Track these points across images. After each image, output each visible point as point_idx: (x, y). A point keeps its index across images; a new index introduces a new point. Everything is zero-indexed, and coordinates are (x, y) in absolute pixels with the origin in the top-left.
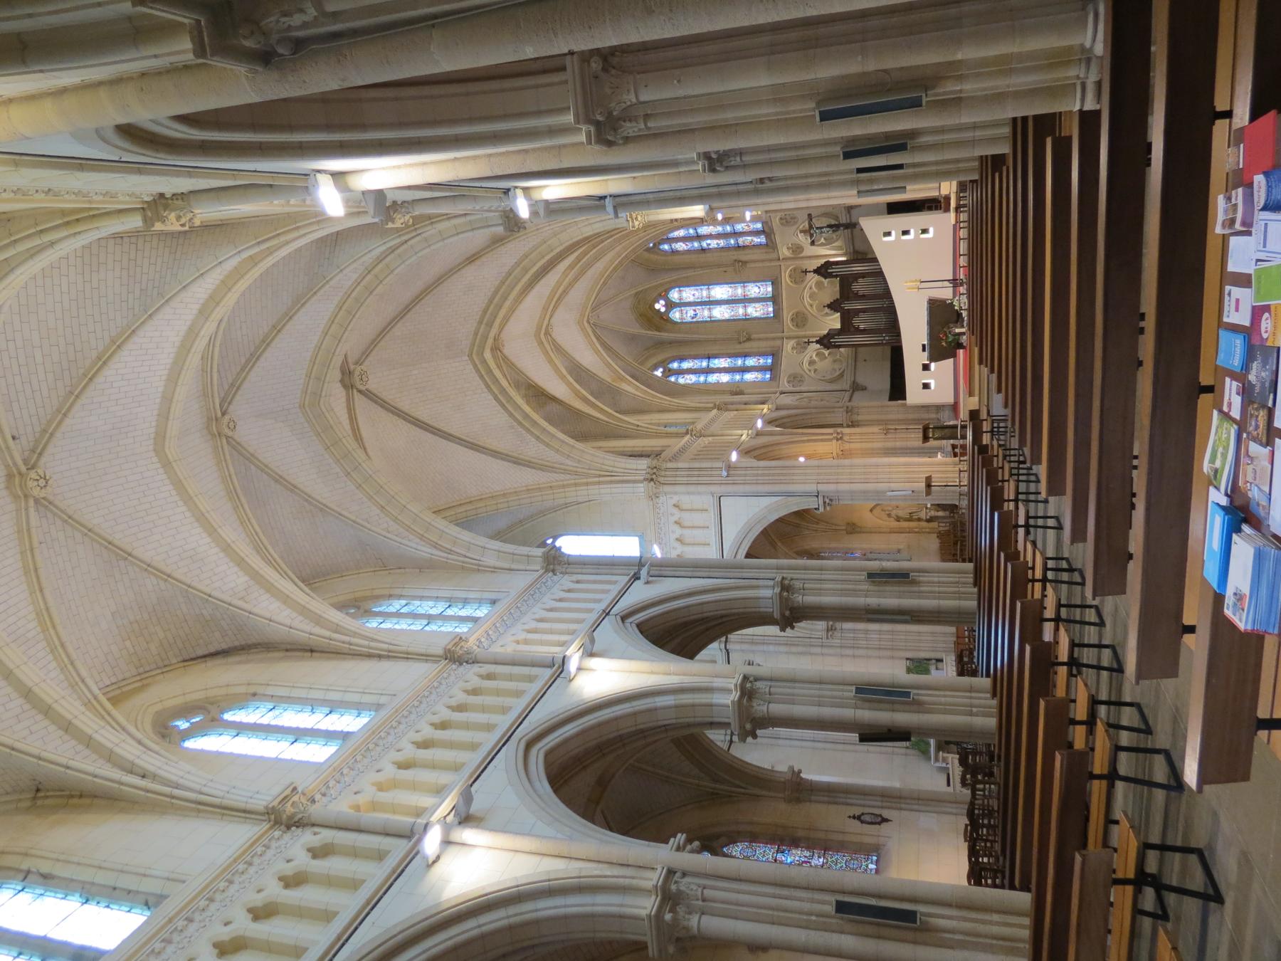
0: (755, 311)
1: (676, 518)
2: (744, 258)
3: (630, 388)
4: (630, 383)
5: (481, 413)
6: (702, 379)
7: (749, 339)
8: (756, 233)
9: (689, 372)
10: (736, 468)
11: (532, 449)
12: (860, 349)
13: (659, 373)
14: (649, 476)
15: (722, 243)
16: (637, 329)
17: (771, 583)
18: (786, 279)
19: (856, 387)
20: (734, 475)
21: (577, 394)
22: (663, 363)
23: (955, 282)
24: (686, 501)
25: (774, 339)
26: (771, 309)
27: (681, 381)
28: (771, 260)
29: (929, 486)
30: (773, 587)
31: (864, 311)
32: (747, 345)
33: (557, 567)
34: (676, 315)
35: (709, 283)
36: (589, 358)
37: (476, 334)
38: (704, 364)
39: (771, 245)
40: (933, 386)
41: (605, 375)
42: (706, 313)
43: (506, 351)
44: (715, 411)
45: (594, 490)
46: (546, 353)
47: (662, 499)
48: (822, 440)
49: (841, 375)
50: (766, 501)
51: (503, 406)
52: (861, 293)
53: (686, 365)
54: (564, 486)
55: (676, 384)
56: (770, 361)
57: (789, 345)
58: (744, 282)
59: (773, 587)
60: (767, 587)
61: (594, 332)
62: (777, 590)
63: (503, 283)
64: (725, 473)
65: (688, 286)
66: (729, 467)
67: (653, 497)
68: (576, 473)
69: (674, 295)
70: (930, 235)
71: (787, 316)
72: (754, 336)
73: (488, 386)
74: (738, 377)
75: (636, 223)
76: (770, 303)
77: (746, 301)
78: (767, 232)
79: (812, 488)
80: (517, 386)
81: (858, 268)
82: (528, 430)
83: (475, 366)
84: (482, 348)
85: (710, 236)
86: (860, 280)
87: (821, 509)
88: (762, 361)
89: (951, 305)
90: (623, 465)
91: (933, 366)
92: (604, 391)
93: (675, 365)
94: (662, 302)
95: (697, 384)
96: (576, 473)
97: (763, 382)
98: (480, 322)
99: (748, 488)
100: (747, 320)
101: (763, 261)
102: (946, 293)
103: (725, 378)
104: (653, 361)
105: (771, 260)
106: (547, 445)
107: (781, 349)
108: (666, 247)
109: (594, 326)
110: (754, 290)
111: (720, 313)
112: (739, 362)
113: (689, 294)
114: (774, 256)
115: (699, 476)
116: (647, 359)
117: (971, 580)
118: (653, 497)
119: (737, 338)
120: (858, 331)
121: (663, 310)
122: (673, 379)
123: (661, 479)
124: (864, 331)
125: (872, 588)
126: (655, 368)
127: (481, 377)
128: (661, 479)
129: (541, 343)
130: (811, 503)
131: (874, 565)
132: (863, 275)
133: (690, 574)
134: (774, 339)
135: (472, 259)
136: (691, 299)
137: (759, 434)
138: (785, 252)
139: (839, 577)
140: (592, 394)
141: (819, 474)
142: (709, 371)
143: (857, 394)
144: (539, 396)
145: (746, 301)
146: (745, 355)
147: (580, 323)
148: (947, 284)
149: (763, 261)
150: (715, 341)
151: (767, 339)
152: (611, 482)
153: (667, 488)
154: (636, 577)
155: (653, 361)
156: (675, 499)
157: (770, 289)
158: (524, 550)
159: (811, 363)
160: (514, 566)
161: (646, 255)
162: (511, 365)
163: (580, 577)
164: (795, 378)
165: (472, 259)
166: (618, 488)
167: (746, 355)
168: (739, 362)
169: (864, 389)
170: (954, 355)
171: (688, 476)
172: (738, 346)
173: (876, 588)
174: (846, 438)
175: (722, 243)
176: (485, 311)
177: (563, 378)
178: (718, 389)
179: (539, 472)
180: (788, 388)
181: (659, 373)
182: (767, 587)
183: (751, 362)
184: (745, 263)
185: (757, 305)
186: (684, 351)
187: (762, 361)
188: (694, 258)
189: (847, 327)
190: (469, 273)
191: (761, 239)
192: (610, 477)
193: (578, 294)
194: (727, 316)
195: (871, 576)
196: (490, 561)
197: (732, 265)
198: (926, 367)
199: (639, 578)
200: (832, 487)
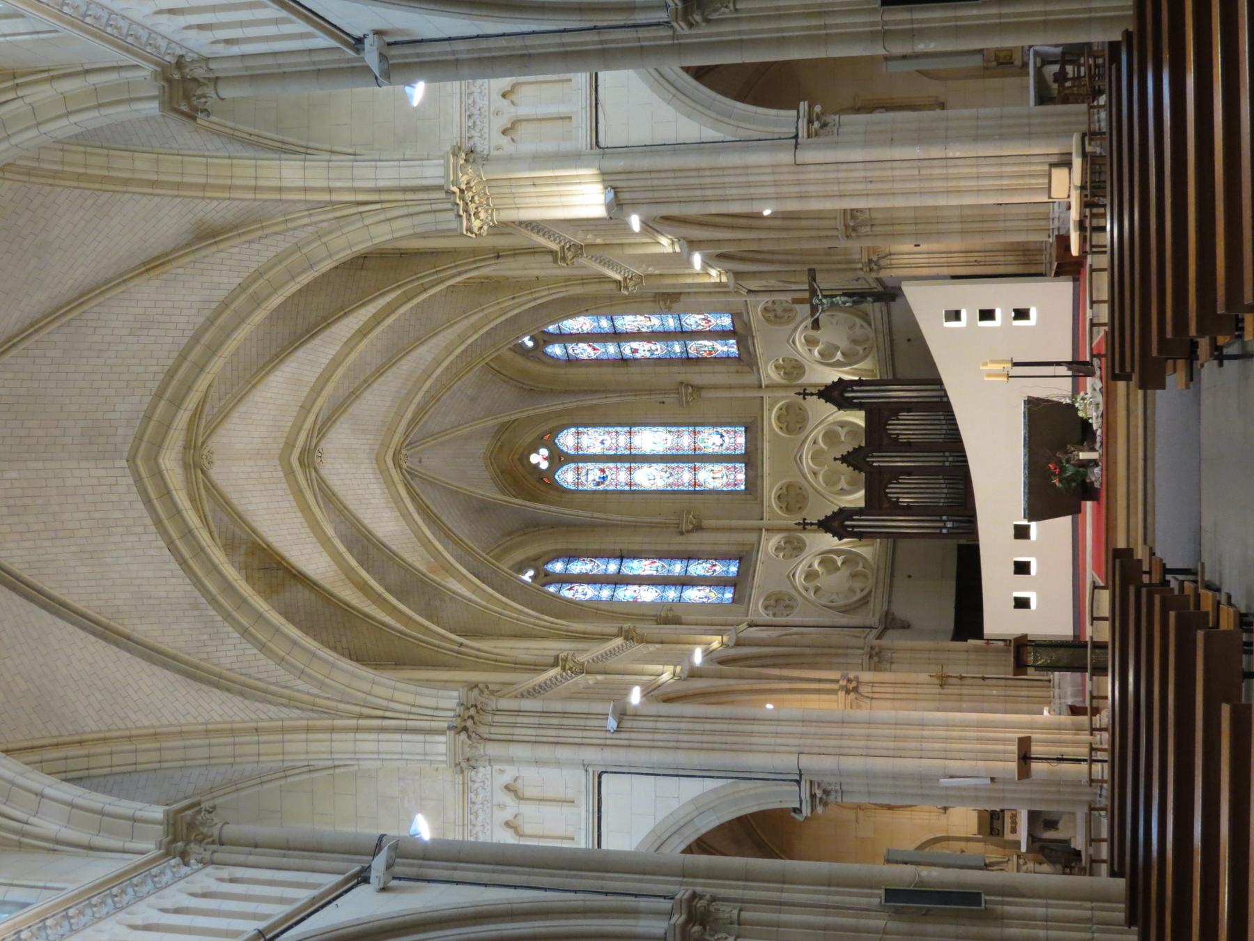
0: (713, 478)
1: (507, 815)
2: (698, 380)
3: (462, 586)
4: (462, 579)
5: (135, 571)
6: (605, 593)
7: (698, 528)
8: (721, 335)
9: (583, 581)
10: (636, 715)
11: (231, 652)
12: (903, 544)
13: (528, 576)
14: (457, 722)
15: (659, 349)
16: (493, 494)
17: (666, 905)
18: (771, 419)
19: (890, 623)
20: (632, 729)
21: (349, 574)
22: (537, 562)
23: (1079, 368)
24: (532, 778)
25: (745, 529)
26: (741, 477)
27: (566, 593)
28: (744, 387)
29: (1025, 758)
30: (671, 914)
31: (908, 472)
32: (696, 538)
33: (193, 847)
34: (566, 477)
35: (632, 423)
36: (386, 522)
37: (148, 417)
38: (612, 567)
39: (746, 359)
40: (1033, 605)
41: (415, 557)
42: (623, 477)
43: (214, 473)
44: (619, 641)
45: (344, 743)
46: (305, 509)
47: (483, 772)
48: (818, 691)
49: (864, 601)
50: (694, 788)
51: (183, 563)
52: (903, 439)
53: (578, 567)
54: (283, 730)
55: (556, 597)
56: (733, 569)
57: (771, 543)
58: (695, 424)
59: (671, 914)
60: (656, 913)
61: (408, 486)
62: (678, 919)
63: (211, 322)
64: (612, 723)
65: (594, 425)
66: (623, 714)
67: (465, 765)
68: (313, 708)
69: (567, 440)
70: (1033, 321)
71: (770, 492)
72: (707, 523)
73: (158, 522)
74: (672, 594)
75: (476, 224)
76: (741, 466)
77: (696, 458)
78: (740, 333)
79: (786, 762)
80: (230, 546)
81: (899, 394)
82: (228, 617)
83: (138, 480)
84: (157, 446)
85: (637, 336)
86: (903, 415)
87: (806, 811)
88: (719, 568)
89: (1071, 408)
90: (411, 698)
91: (1034, 526)
92: (414, 587)
93: (558, 567)
94: (544, 452)
95: (596, 601)
96: (313, 708)
97: (718, 607)
98: (159, 395)
99: (656, 757)
100: (697, 493)
101: (730, 387)
102: (1058, 388)
103: (648, 594)
104: (519, 556)
105: (744, 387)
106: (263, 647)
107: (754, 548)
108: (556, 350)
109: (410, 476)
110: (711, 440)
111: (649, 478)
112: (677, 568)
113: (594, 440)
114: (750, 379)
115: (560, 727)
116: (507, 551)
117: (1122, 916)
118: (465, 765)
119: (676, 524)
120: (897, 509)
121: (544, 465)
122: (552, 589)
123: (483, 730)
124: (908, 510)
125: (892, 925)
126: (521, 569)
127: (148, 502)
128: (483, 730)
129: (289, 473)
130: (784, 798)
131: (903, 874)
132: (908, 407)
133: (485, 877)
134: (745, 529)
135: (153, 265)
136: (597, 450)
137: (694, 674)
138: (770, 373)
139: (822, 898)
140: (388, 590)
141: (802, 735)
142: (619, 580)
143: (890, 633)
144: (272, 570)
145: (696, 458)
146: (689, 557)
147: (379, 459)
148: (1063, 370)
149: (730, 387)
150: (634, 527)
151: (730, 529)
152: (383, 730)
153: (492, 749)
154: (362, 878)
155: (519, 556)
156: (510, 773)
157: (741, 440)
158: (126, 807)
159: (811, 575)
160: (100, 841)
161: (521, 362)
162: (224, 504)
163: (240, 872)
164: (778, 602)
165: (153, 265)
166: (393, 744)
167: (689, 557)
168: (677, 568)
169: (905, 626)
170: (1075, 510)
171: (540, 726)
172: (680, 539)
173: (903, 926)
174: (864, 690)
175: (659, 349)
176: (171, 374)
177: (325, 542)
178: (635, 612)
179: (238, 700)
180: (765, 617)
181: (528, 576)
182: (656, 913)
183: (698, 569)
184: (698, 389)
185: (717, 467)
186: (580, 543)
187: (719, 568)
188: (607, 373)
189: (877, 502)
190: (146, 292)
191: (729, 348)
192: (381, 720)
193: (378, 401)
194: (660, 484)
195: (893, 895)
196: (50, 825)
197: (675, 392)
198: (1021, 533)
199: (366, 880)
200: (828, 763)
